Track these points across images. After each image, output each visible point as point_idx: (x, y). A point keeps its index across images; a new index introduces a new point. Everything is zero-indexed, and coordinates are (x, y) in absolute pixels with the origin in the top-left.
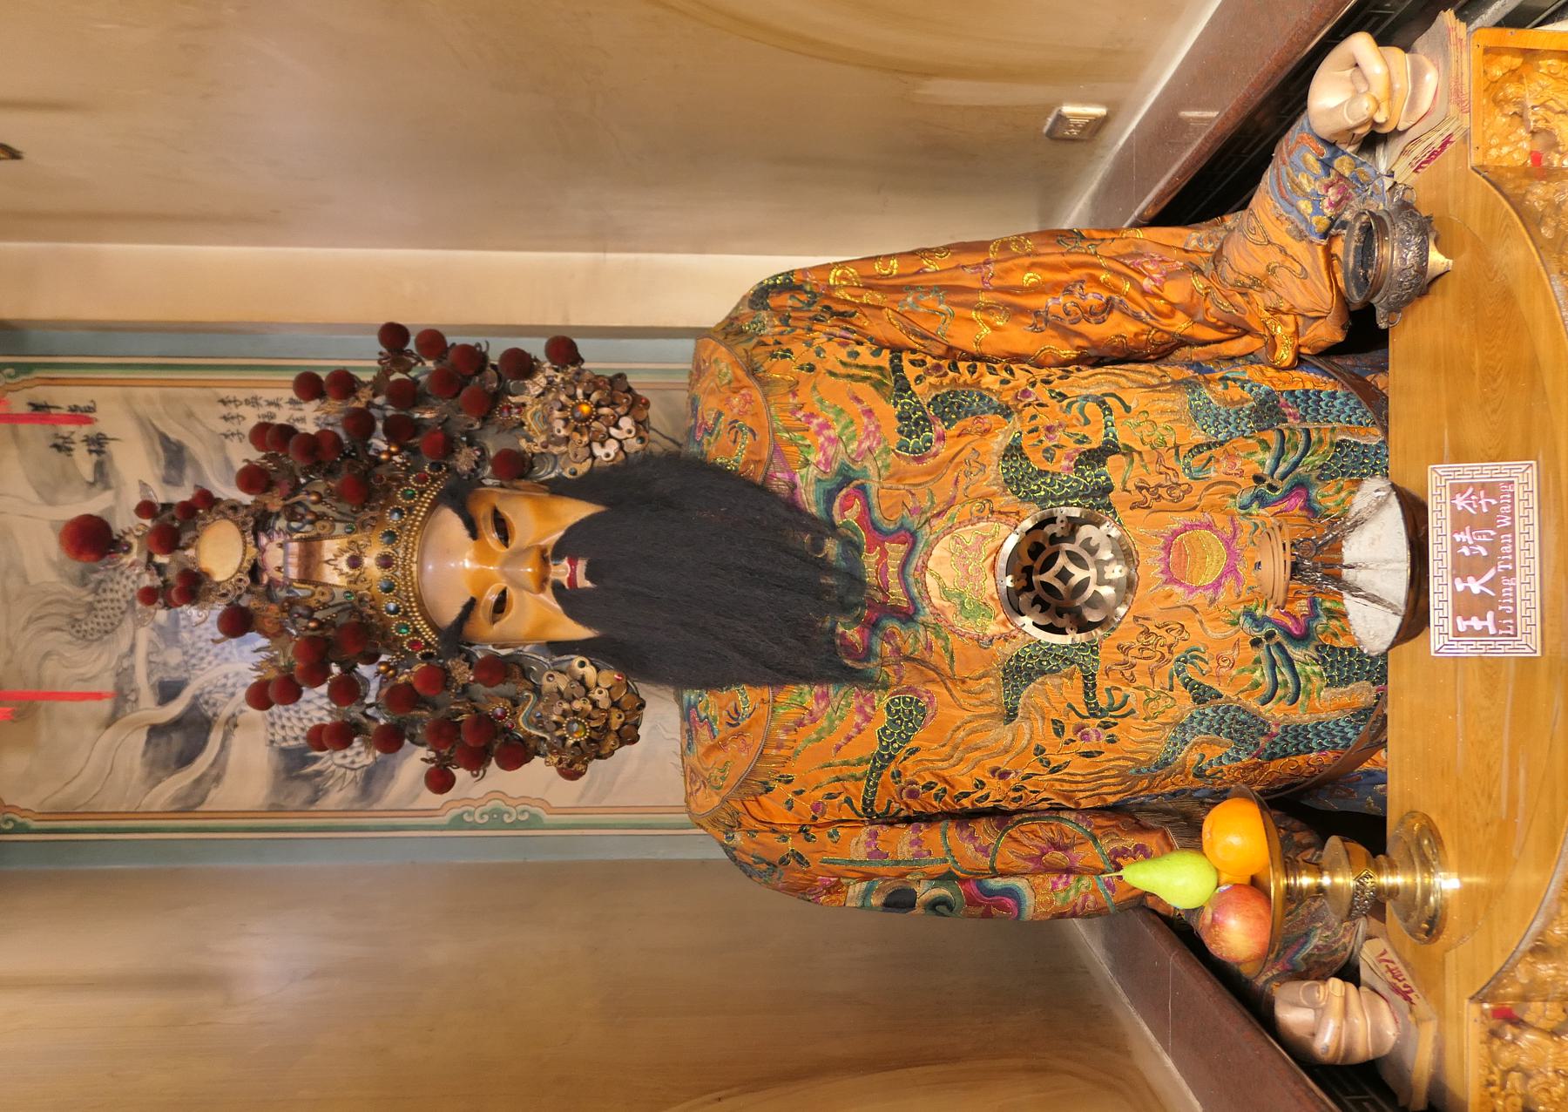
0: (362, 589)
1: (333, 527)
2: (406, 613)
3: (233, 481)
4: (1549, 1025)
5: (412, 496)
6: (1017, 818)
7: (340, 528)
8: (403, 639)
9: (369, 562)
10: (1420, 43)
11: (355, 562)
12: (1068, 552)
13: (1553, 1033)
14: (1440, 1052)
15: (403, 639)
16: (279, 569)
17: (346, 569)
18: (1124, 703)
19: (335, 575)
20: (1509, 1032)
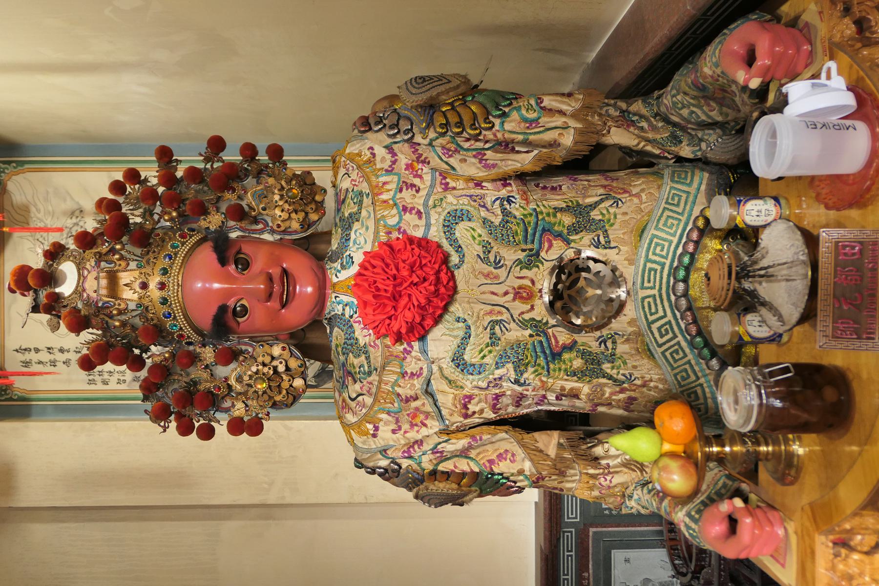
0: (146, 302)
1: (128, 264)
2: (175, 317)
3: (220, 304)
4: (866, 549)
5: (177, 247)
6: (27, 166)
7: (133, 265)
8: (174, 333)
9: (153, 285)
10: (815, 233)
11: (144, 286)
12: (585, 278)
13: (867, 553)
14: (798, 462)
15: (174, 333)
16: (95, 291)
17: (138, 289)
18: (600, 344)
19: (130, 296)
20: (843, 551)
